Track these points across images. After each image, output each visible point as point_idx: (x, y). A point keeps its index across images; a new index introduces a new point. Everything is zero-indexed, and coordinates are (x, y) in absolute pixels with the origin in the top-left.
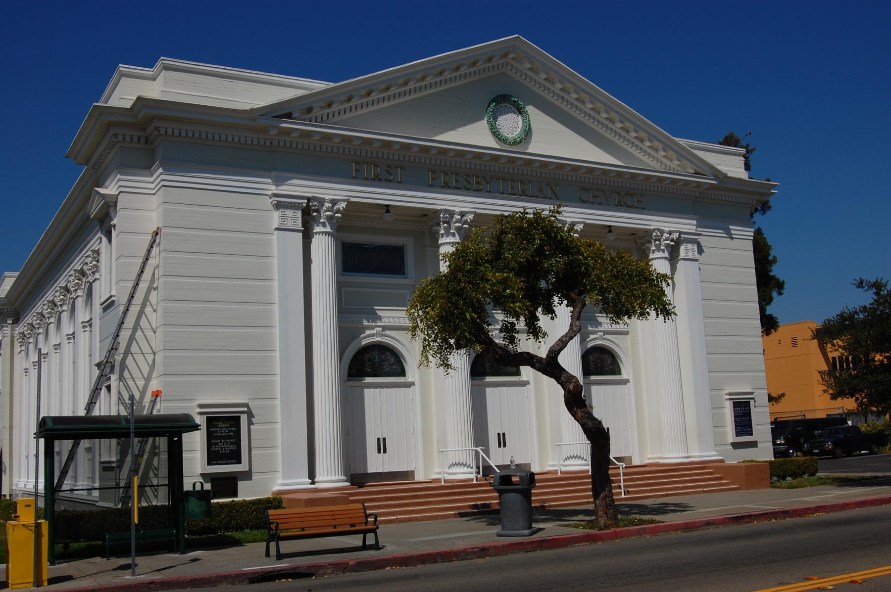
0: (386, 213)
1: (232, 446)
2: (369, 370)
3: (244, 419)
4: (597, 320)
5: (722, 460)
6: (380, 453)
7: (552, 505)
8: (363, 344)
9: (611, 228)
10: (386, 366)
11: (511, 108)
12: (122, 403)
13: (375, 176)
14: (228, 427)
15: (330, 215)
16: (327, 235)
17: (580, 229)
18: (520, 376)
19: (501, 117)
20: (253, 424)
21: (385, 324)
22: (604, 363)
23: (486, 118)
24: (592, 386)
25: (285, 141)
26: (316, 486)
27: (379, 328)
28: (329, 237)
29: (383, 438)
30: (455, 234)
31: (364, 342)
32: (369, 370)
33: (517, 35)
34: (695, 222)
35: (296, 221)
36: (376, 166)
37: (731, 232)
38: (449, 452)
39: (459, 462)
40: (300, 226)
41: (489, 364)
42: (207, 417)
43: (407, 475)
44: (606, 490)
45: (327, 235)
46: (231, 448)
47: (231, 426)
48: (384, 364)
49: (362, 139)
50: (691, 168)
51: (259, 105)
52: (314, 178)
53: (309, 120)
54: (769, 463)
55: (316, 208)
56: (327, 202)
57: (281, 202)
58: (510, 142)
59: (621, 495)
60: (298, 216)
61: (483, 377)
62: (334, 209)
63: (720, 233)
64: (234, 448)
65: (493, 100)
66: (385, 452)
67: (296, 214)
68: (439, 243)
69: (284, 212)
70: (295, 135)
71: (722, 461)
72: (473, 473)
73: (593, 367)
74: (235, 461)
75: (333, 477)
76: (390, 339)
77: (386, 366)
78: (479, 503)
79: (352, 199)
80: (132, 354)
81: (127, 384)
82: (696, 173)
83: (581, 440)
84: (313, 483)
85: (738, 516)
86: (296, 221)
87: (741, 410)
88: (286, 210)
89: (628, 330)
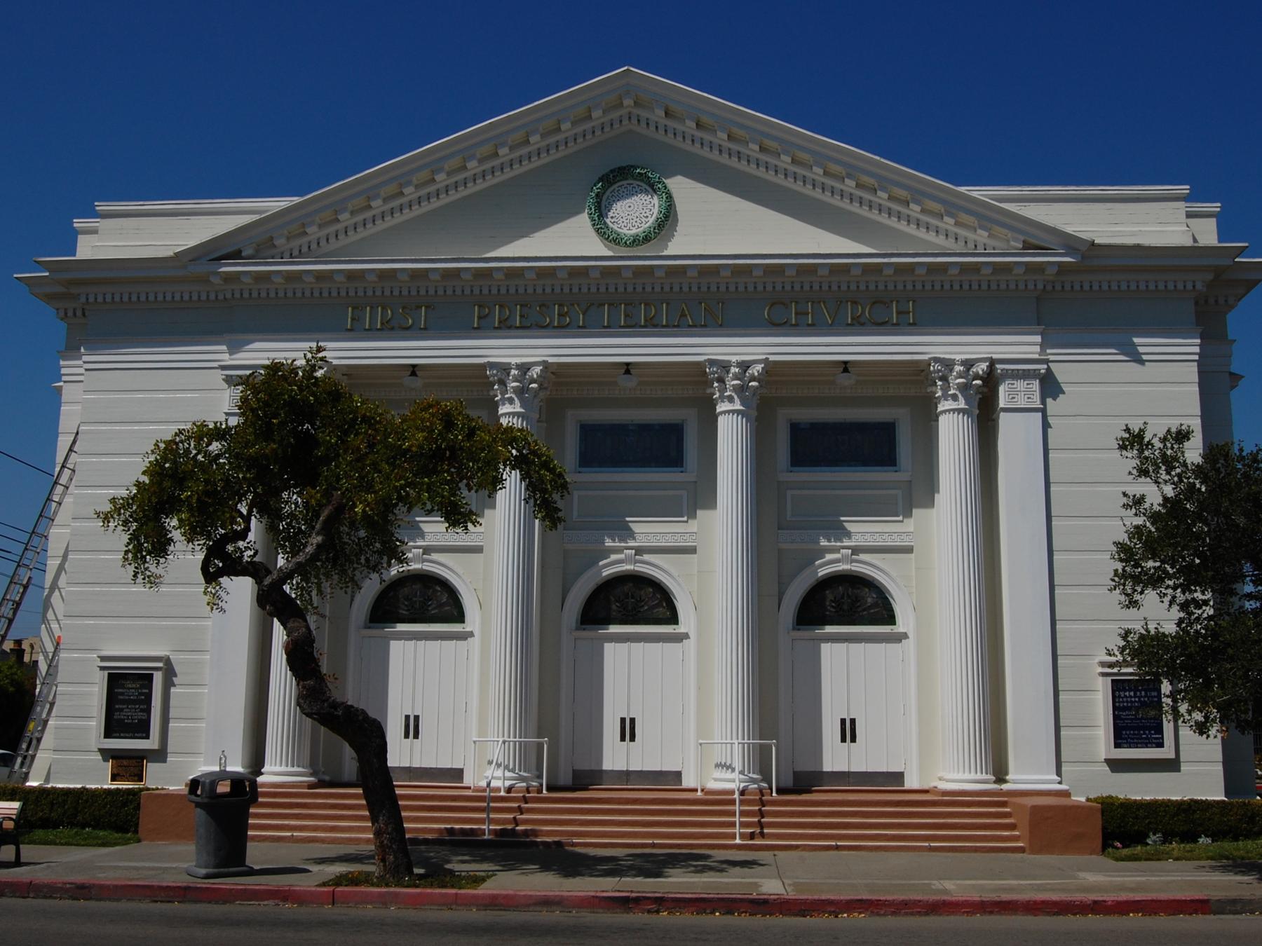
0: (624, 374)
1: (141, 714)
2: (404, 612)
3: (158, 678)
4: (844, 528)
5: (1067, 791)
6: (845, 742)
7: (657, 844)
8: (820, 574)
9: (847, 366)
10: (434, 606)
11: (621, 186)
12: (42, 652)
13: (852, 319)
14: (138, 689)
15: (963, 383)
16: (516, 417)
17: (758, 372)
18: (895, 624)
19: (619, 204)
20: (175, 686)
21: (431, 543)
22: (859, 604)
23: (586, 211)
24: (822, 645)
25: (942, 281)
26: (1005, 787)
27: (631, 551)
28: (964, 416)
29: (851, 719)
30: (513, 399)
31: (822, 572)
32: (404, 612)
33: (626, 68)
34: (1038, 339)
35: (1032, 396)
36: (855, 303)
37: (1137, 350)
38: (716, 745)
39: (725, 763)
40: (1038, 402)
41: (618, 604)
42: (109, 674)
43: (898, 777)
44: (380, 821)
45: (516, 417)
46: (139, 717)
47: (142, 687)
48: (430, 603)
49: (1059, 266)
50: (1015, 240)
51: (187, 245)
52: (298, 337)
53: (280, 256)
54: (1102, 804)
55: (940, 374)
56: (958, 365)
57: (231, 376)
58: (626, 243)
59: (736, 838)
60: (1034, 389)
61: (393, 625)
62: (969, 375)
63: (1111, 353)
64: (144, 718)
65: (601, 179)
66: (416, 736)
67: (1031, 386)
68: (939, 410)
69: (1013, 384)
70: (986, 271)
71: (1066, 794)
72: (734, 782)
73: (832, 609)
74: (144, 735)
75: (979, 774)
76: (872, 569)
77: (434, 606)
78: (457, 827)
79: (772, 358)
80: (59, 589)
81: (50, 627)
82: (1027, 246)
83: (496, 735)
84: (1000, 779)
85: (629, 897)
86: (1032, 396)
87: (1135, 697)
88: (1015, 382)
89: (912, 544)
